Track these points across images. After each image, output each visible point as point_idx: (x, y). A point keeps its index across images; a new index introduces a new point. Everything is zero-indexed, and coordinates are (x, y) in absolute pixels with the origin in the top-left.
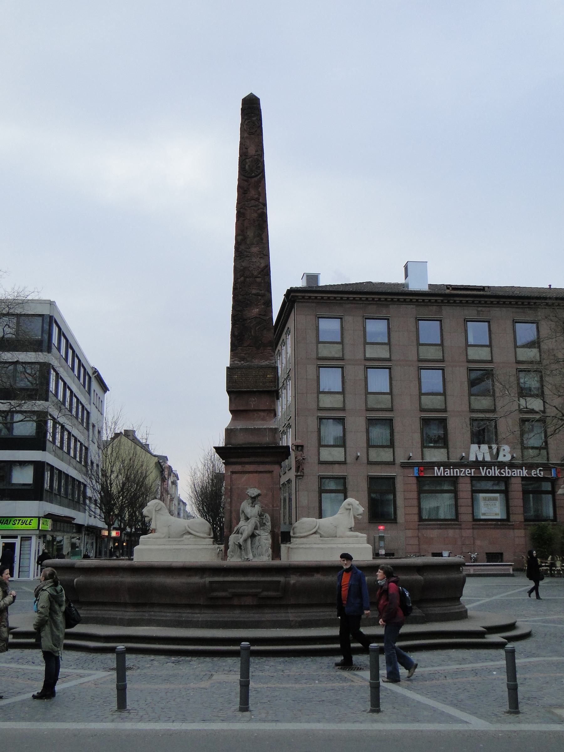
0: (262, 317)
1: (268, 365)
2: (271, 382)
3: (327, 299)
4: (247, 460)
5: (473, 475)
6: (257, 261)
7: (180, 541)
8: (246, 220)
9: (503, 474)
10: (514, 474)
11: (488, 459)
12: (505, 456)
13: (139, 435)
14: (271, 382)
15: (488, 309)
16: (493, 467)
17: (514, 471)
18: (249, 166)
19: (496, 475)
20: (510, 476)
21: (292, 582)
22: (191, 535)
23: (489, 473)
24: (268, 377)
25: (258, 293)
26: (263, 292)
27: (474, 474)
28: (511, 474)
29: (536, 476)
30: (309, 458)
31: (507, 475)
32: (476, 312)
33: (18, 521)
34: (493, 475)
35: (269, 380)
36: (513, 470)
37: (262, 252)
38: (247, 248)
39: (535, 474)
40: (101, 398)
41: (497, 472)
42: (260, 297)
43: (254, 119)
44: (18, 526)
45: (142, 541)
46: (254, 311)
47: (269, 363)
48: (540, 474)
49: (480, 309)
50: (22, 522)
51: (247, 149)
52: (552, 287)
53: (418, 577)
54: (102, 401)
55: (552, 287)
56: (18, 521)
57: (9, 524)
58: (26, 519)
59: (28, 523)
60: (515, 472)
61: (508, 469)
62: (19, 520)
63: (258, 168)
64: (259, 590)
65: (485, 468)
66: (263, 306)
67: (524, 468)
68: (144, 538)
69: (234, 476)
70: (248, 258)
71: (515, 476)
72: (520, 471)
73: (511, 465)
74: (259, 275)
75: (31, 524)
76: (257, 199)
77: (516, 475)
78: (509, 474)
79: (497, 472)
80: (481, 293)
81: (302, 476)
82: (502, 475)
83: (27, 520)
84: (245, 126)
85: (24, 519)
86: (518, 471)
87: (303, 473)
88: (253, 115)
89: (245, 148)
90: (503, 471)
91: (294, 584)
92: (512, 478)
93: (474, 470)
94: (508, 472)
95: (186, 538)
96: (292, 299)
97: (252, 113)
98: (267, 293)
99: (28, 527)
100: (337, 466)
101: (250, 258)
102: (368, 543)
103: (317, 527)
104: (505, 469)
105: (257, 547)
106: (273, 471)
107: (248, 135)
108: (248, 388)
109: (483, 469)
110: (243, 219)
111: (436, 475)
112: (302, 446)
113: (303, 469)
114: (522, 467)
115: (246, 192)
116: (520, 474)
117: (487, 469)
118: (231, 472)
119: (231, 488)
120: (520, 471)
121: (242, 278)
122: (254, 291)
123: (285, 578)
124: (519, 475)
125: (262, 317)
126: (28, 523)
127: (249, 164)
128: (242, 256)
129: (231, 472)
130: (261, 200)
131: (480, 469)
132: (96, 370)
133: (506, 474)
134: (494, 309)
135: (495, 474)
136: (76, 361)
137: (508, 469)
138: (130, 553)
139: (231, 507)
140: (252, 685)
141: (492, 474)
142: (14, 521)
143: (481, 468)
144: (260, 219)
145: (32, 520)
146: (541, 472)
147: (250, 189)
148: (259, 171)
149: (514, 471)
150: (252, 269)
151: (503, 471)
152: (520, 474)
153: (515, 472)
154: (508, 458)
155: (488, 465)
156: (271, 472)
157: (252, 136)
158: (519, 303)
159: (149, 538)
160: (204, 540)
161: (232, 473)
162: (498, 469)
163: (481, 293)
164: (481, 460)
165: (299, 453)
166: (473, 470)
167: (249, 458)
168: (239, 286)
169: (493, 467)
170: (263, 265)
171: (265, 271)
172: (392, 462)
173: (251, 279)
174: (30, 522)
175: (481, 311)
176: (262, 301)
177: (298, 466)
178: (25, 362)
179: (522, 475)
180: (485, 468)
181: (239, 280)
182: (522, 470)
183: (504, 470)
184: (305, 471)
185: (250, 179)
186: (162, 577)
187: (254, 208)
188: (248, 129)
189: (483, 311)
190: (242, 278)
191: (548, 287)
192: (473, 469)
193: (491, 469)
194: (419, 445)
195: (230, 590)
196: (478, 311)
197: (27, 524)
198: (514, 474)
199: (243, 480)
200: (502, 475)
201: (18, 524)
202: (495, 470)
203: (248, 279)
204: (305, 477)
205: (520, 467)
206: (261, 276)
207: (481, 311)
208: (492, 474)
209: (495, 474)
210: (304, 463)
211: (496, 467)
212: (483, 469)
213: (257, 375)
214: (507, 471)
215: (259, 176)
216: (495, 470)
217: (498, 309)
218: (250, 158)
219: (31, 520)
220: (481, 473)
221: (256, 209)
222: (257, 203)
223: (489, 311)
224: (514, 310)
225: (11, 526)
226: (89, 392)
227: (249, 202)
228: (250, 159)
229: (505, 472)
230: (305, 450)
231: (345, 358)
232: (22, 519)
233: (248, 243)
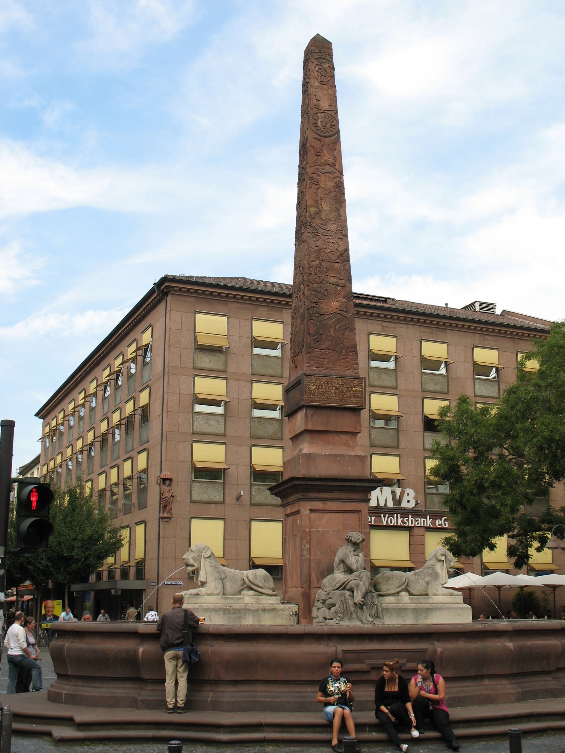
0: (343, 313)
2: (357, 397)
3: (202, 293)
4: (328, 495)
5: (373, 523)
6: (335, 242)
8: (320, 189)
9: (406, 523)
10: (418, 524)
11: (390, 504)
12: (409, 501)
14: (357, 397)
15: (393, 325)
16: (395, 515)
17: (418, 520)
18: (322, 122)
19: (399, 524)
20: (414, 526)
21: (439, 650)
22: (253, 591)
23: (391, 522)
24: (354, 391)
25: (337, 282)
26: (343, 281)
27: (374, 522)
28: (415, 524)
29: (440, 526)
30: (178, 495)
31: (410, 525)
32: (381, 327)
34: (396, 524)
35: (355, 394)
36: (417, 519)
37: (341, 231)
38: (323, 224)
39: (439, 525)
41: (400, 521)
42: (339, 288)
43: (326, 66)
46: (333, 305)
48: (445, 524)
49: (385, 324)
51: (319, 101)
52: (449, 306)
53: (510, 645)
55: (449, 306)
60: (419, 522)
61: (411, 518)
63: (333, 127)
64: (403, 661)
65: (387, 515)
66: (343, 300)
67: (428, 516)
69: (313, 515)
70: (324, 237)
71: (419, 526)
72: (424, 521)
73: (415, 513)
74: (338, 261)
76: (333, 165)
77: (419, 525)
78: (391, 523)
79: (400, 521)
80: (381, 304)
81: (170, 518)
82: (405, 525)
84: (315, 72)
86: (422, 520)
87: (171, 514)
88: (324, 61)
89: (317, 100)
90: (406, 520)
91: (442, 652)
92: (415, 527)
93: (375, 517)
94: (412, 521)
96: (165, 290)
97: (324, 59)
98: (347, 284)
100: (213, 505)
101: (326, 237)
102: (465, 602)
103: (406, 583)
104: (408, 518)
105: (371, 607)
106: (360, 511)
107: (319, 85)
109: (385, 517)
110: (317, 187)
112: (171, 480)
113: (171, 510)
114: (427, 515)
115: (319, 154)
116: (424, 524)
117: (388, 517)
118: (309, 510)
119: (310, 531)
120: (424, 521)
121: (317, 262)
122: (332, 280)
124: (422, 525)
125: (343, 313)
127: (322, 120)
128: (316, 233)
129: (309, 510)
130: (337, 167)
131: (381, 516)
133: (409, 524)
134: (401, 325)
135: (397, 523)
137: (411, 518)
139: (310, 554)
141: (394, 523)
143: (382, 515)
144: (337, 190)
146: (445, 522)
147: (325, 151)
148: (334, 132)
149: (418, 520)
150: (329, 251)
151: (406, 520)
152: (424, 524)
153: (419, 522)
154: (412, 505)
155: (390, 512)
156: (358, 512)
157: (325, 87)
158: (428, 321)
160: (269, 597)
161: (311, 512)
162: (400, 518)
163: (381, 304)
164: (383, 506)
165: (165, 488)
166: (373, 518)
167: (333, 492)
168: (313, 270)
169: (395, 515)
170: (341, 249)
171: (344, 255)
173: (328, 264)
175: (387, 327)
176: (343, 294)
177: (165, 505)
179: (426, 525)
180: (387, 515)
181: (314, 263)
182: (426, 519)
183: (407, 519)
184: (173, 511)
186: (235, 646)
187: (330, 175)
188: (320, 77)
189: (388, 327)
190: (317, 262)
191: (445, 306)
192: (374, 516)
193: (394, 517)
196: (383, 327)
198: (418, 524)
199: (324, 520)
200: (405, 525)
202: (397, 517)
203: (324, 263)
204: (173, 520)
205: (423, 515)
206: (340, 261)
207: (387, 327)
208: (394, 523)
209: (397, 523)
210: (172, 502)
211: (399, 515)
212: (385, 517)
213: (340, 387)
214: (410, 519)
215: (334, 137)
216: (397, 517)
217: (405, 326)
218: (323, 112)
220: (382, 523)
221: (332, 176)
222: (333, 169)
223: (395, 328)
224: (422, 328)
227: (323, 167)
228: (323, 114)
229: (408, 520)
230: (174, 484)
231: (228, 371)
233: (323, 217)
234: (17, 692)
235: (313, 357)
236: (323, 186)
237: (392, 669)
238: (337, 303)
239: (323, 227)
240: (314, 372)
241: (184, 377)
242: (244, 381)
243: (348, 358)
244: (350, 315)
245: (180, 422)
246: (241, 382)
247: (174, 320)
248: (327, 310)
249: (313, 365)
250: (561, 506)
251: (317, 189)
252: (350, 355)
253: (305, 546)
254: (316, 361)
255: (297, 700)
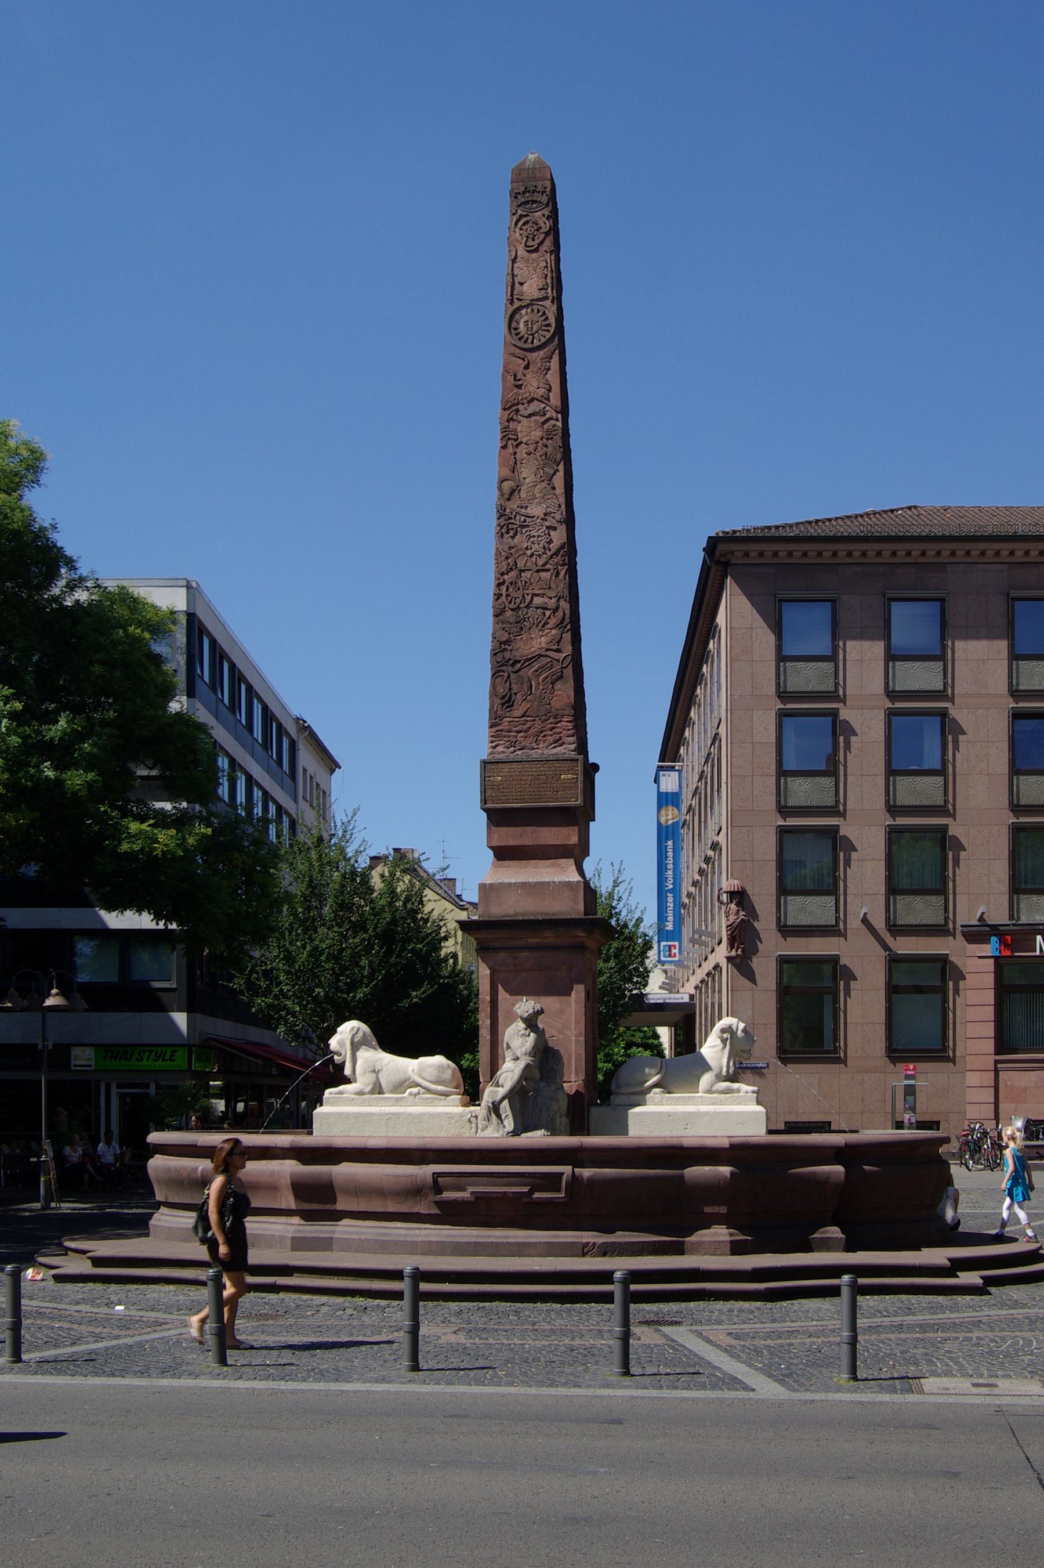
1: (564, 753)
7: (398, 1100)
13: (598, 777)
33: (147, 1054)
40: (321, 787)
44: (148, 1064)
45: (329, 1098)
47: (565, 749)
50: (155, 1056)
54: (324, 792)
56: (147, 1054)
57: (130, 1060)
58: (164, 1049)
59: (167, 1057)
62: (150, 1052)
68: (331, 1094)
75: (174, 1060)
83: (166, 1051)
85: (159, 1049)
95: (410, 1094)
99: (167, 1065)
108: (522, 801)
111: (1038, 953)
123: (948, 1197)
125: (551, 653)
126: (167, 1057)
132: (306, 725)
136: (257, 709)
138: (306, 1124)
140: (423, 1331)
142: (140, 1054)
145: (176, 1051)
159: (340, 1093)
172: (940, 925)
174: (172, 1055)
178: (557, 210)
185: (528, 354)
194: (1004, 887)
195: (471, 1189)
197: (166, 1060)
201: (148, 1060)
219: (173, 1052)
225: (133, 1064)
226: (293, 775)
232: (155, 1049)
234: (292, 1250)
235: (501, 731)
236: (524, 440)
237: (208, 1194)
238: (543, 638)
239: (523, 510)
240: (501, 756)
241: (760, 712)
242: (872, 708)
243: (558, 727)
244: (564, 655)
245: (756, 793)
246: (866, 711)
247: (739, 613)
248: (526, 652)
249: (501, 745)
250: (782, 939)
251: (517, 446)
252: (561, 721)
253: (484, 1022)
254: (505, 736)
255: (379, 1238)
